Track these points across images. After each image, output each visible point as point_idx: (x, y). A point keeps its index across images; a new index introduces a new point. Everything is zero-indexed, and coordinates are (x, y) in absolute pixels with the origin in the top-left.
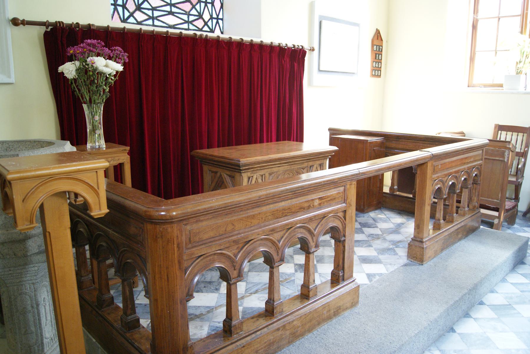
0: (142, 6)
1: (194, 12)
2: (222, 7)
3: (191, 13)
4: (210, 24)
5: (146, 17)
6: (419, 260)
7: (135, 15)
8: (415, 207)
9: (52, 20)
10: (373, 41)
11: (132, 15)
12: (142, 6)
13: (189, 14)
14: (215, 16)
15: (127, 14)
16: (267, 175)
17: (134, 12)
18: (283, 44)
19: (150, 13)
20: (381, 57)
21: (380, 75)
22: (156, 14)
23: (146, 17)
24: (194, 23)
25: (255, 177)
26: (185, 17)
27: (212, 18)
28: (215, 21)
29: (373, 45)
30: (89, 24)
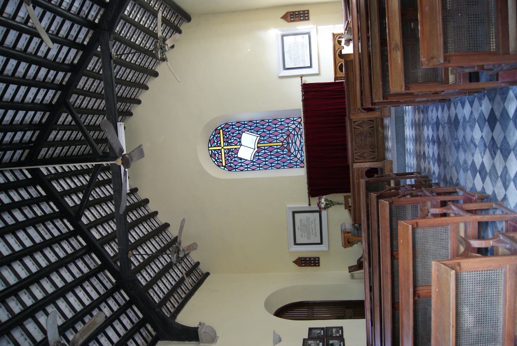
0: (295, 155)
1: (293, 132)
2: (288, 119)
3: (294, 134)
4: (296, 124)
5: (299, 153)
6: (445, 15)
7: (299, 158)
8: (345, 137)
9: (307, 195)
10: (288, 22)
11: (299, 159)
12: (295, 155)
13: (294, 135)
14: (293, 122)
15: (299, 161)
16: (356, 151)
17: (298, 158)
18: (301, 89)
19: (297, 152)
20: (297, 11)
21: (307, 10)
22: (297, 149)
23: (299, 153)
24: (297, 132)
25: (356, 157)
26: (296, 136)
27: (294, 124)
28: (295, 122)
29: (291, 21)
30: (302, 101)
